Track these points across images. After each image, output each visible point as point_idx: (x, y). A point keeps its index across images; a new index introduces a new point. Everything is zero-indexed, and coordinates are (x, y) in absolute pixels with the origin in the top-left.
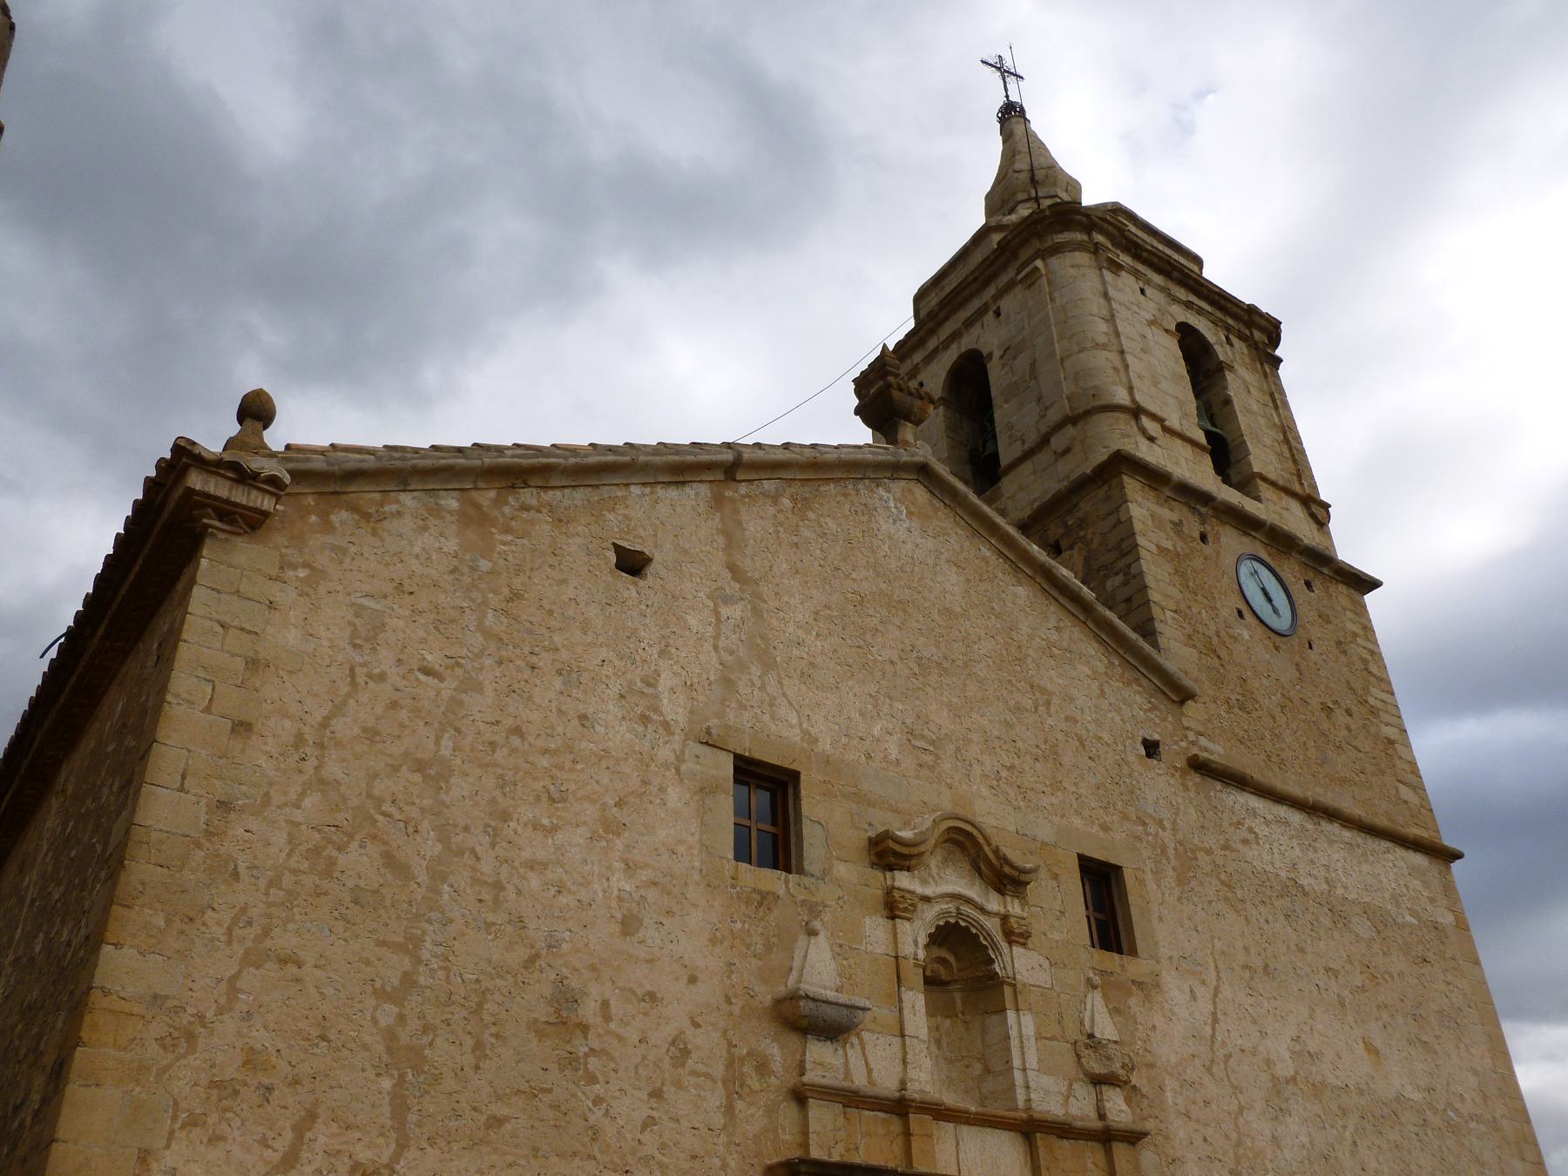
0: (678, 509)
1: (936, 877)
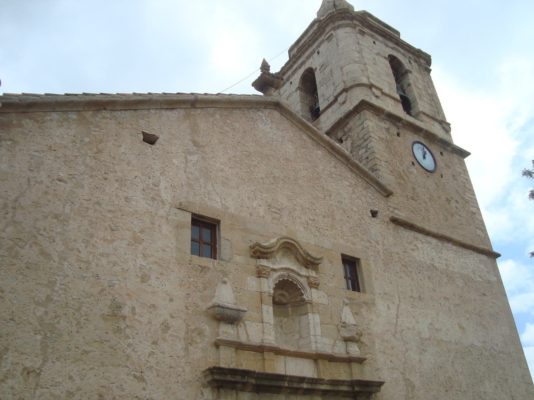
0: (171, 119)
1: (279, 262)
